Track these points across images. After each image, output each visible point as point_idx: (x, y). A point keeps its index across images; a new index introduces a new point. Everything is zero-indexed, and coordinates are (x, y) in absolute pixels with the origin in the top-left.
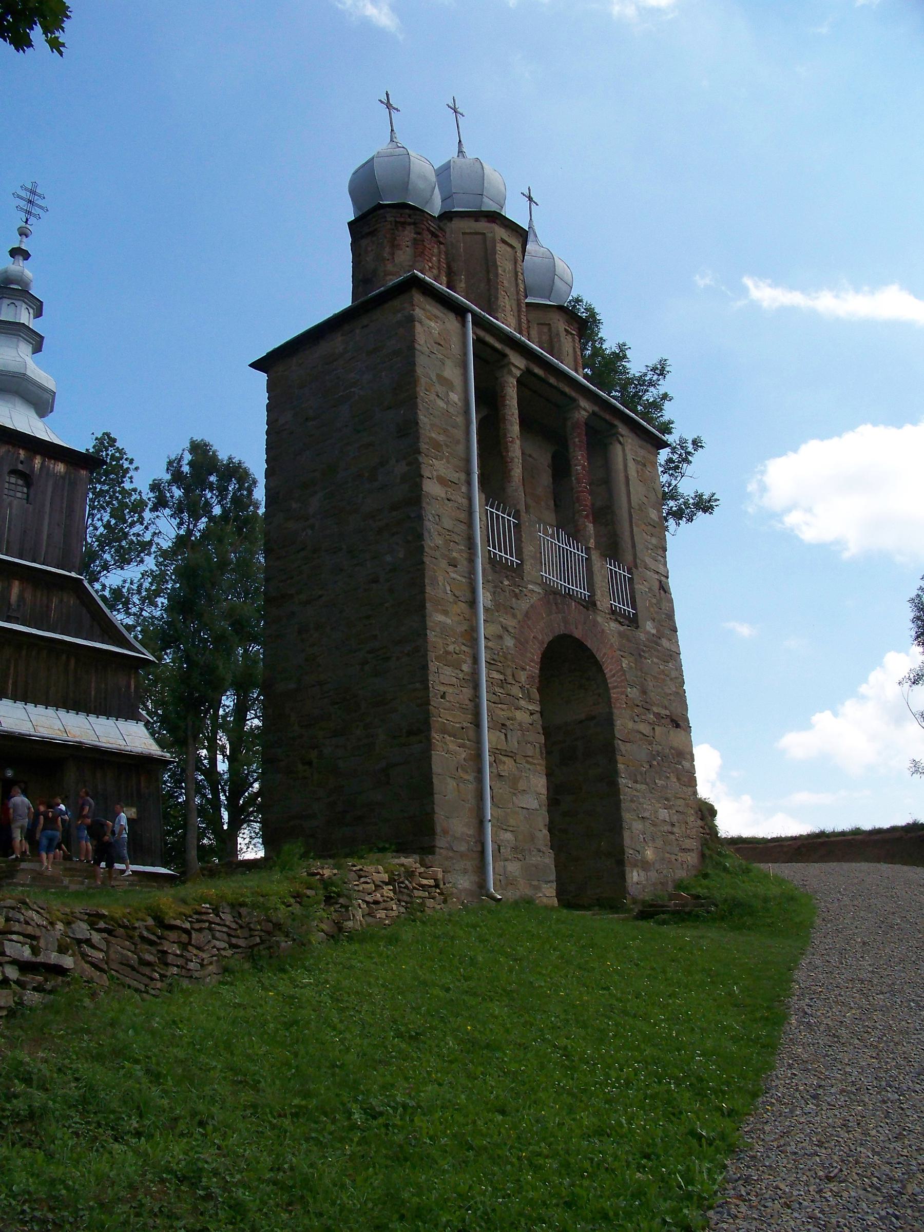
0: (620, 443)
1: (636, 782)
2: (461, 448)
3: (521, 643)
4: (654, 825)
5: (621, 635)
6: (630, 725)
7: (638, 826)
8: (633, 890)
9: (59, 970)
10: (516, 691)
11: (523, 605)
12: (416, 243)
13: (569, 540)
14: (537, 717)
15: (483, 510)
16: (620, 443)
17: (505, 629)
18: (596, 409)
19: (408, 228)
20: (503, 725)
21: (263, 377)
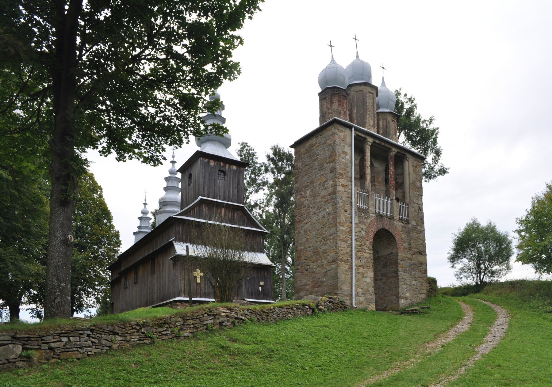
2: (349, 174)
3: (367, 233)
4: (410, 286)
5: (402, 226)
6: (404, 255)
7: (405, 286)
8: (401, 305)
9: (242, 319)
10: (365, 247)
11: (369, 221)
12: (339, 101)
14: (371, 255)
17: (362, 229)
18: (398, 150)
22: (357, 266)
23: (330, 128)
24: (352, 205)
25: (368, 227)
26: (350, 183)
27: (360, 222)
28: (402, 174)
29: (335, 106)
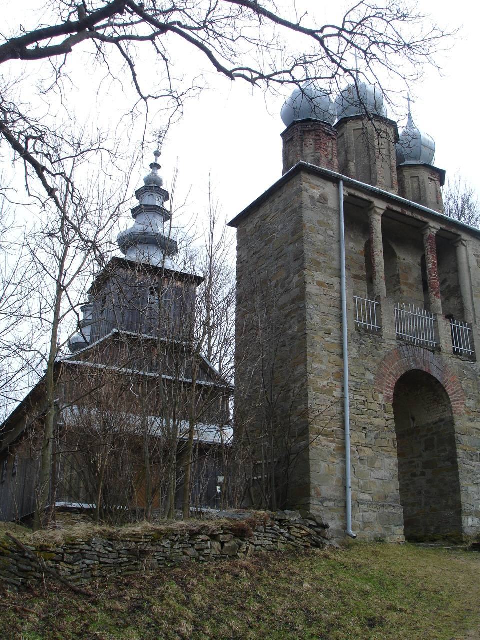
0: (464, 245)
1: (472, 460)
3: (380, 376)
8: (468, 530)
11: (382, 353)
13: (424, 312)
14: (391, 422)
15: (351, 299)
16: (464, 245)
19: (312, 133)
20: (364, 428)
21: (234, 230)
22: (358, 446)
23: (293, 181)
24: (341, 322)
25: (380, 365)
26: (335, 280)
27: (363, 356)
28: (457, 270)
29: (309, 150)
